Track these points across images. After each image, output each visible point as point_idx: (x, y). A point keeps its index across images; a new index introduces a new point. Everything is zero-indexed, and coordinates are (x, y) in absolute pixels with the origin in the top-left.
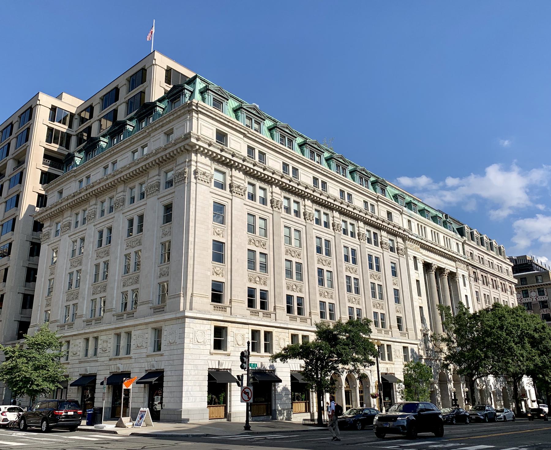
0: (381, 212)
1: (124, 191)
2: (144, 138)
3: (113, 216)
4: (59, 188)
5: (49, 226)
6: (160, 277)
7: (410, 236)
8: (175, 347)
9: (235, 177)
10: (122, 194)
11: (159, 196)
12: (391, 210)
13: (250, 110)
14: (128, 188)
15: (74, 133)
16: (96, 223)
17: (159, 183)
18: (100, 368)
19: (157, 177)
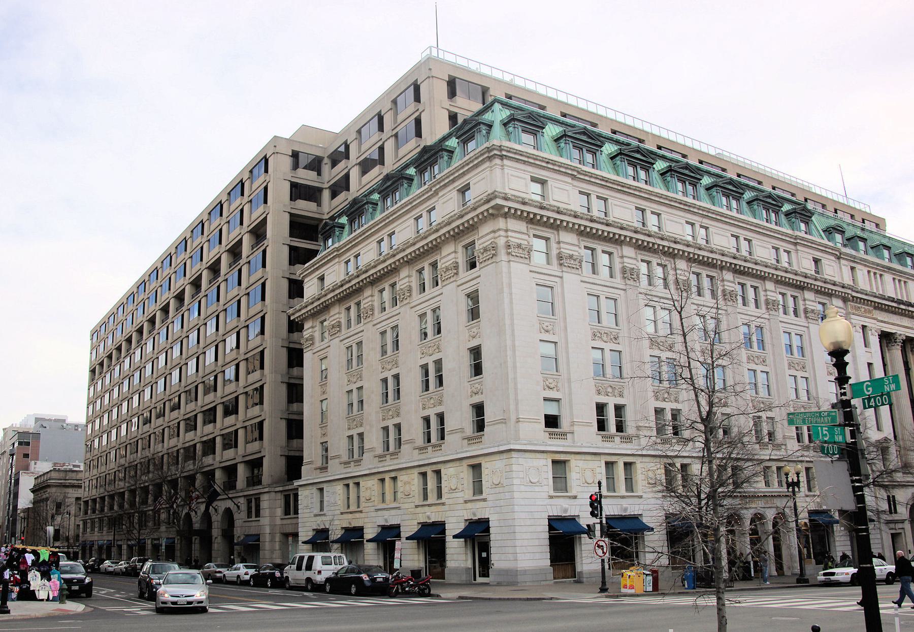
0: (804, 263)
1: (409, 276)
2: (429, 198)
3: (397, 312)
4: (318, 273)
5: (312, 327)
6: (471, 396)
7: (854, 294)
8: (501, 490)
9: (564, 242)
10: (407, 280)
11: (459, 283)
12: (818, 255)
13: (577, 136)
14: (414, 272)
15: (327, 186)
16: (375, 322)
17: (457, 263)
18: (405, 517)
19: (453, 255)
